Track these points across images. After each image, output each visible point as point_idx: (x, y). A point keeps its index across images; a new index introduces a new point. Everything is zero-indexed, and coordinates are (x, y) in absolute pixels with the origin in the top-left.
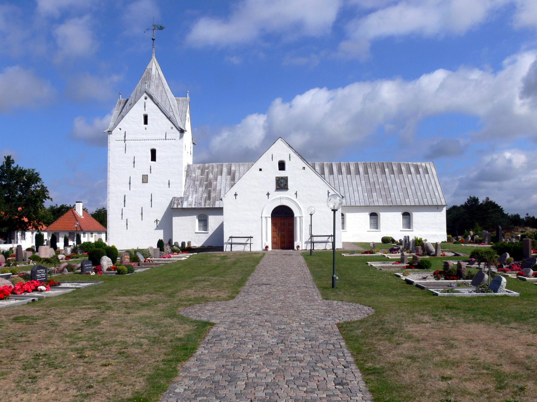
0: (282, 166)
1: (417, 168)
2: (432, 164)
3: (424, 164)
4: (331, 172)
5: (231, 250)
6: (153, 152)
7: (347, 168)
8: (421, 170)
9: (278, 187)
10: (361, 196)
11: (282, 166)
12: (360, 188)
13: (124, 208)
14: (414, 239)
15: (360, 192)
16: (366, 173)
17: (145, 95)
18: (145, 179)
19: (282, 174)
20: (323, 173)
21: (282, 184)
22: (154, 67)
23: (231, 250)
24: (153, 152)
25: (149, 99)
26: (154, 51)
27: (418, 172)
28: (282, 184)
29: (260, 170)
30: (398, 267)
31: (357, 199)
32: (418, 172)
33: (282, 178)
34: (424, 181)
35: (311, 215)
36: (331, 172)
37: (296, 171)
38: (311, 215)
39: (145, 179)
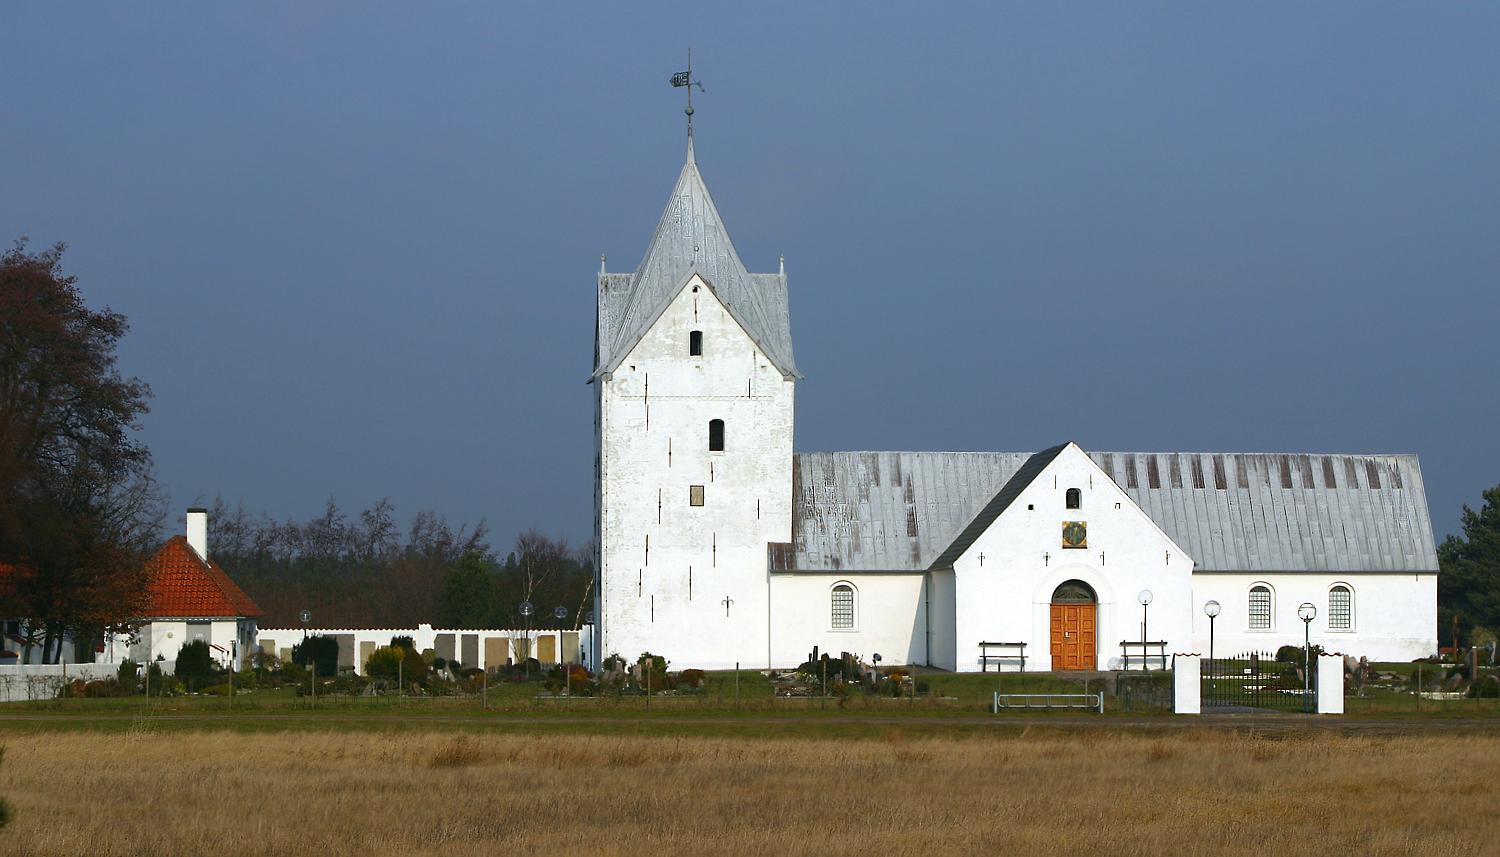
0: (1073, 498)
1: (1372, 471)
2: (1415, 461)
3: (1392, 461)
4: (1154, 482)
5: (984, 670)
6: (717, 429)
7: (1194, 469)
8: (1382, 476)
9: (1067, 544)
10: (1230, 547)
11: (1073, 498)
12: (1227, 526)
13: (643, 567)
14: (351, 518)
15: (1228, 535)
16: (1243, 483)
17: (696, 281)
18: (697, 496)
19: (1073, 516)
20: (1133, 483)
21: (1074, 536)
22: (692, 197)
23: (984, 670)
24: (717, 429)
25: (704, 290)
26: (691, 145)
27: (1374, 482)
28: (1074, 536)
29: (1031, 507)
30: (1302, 721)
31: (1219, 551)
32: (1374, 482)
33: (1075, 524)
34: (1389, 507)
35: (1212, 617)
36: (1154, 482)
37: (1105, 500)
38: (1212, 617)
39: (697, 496)
